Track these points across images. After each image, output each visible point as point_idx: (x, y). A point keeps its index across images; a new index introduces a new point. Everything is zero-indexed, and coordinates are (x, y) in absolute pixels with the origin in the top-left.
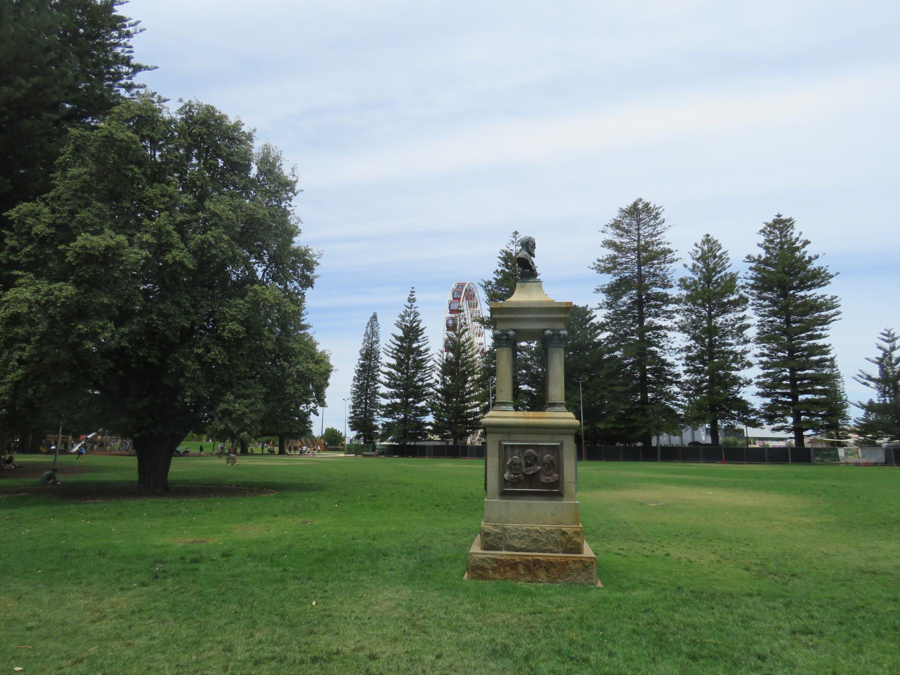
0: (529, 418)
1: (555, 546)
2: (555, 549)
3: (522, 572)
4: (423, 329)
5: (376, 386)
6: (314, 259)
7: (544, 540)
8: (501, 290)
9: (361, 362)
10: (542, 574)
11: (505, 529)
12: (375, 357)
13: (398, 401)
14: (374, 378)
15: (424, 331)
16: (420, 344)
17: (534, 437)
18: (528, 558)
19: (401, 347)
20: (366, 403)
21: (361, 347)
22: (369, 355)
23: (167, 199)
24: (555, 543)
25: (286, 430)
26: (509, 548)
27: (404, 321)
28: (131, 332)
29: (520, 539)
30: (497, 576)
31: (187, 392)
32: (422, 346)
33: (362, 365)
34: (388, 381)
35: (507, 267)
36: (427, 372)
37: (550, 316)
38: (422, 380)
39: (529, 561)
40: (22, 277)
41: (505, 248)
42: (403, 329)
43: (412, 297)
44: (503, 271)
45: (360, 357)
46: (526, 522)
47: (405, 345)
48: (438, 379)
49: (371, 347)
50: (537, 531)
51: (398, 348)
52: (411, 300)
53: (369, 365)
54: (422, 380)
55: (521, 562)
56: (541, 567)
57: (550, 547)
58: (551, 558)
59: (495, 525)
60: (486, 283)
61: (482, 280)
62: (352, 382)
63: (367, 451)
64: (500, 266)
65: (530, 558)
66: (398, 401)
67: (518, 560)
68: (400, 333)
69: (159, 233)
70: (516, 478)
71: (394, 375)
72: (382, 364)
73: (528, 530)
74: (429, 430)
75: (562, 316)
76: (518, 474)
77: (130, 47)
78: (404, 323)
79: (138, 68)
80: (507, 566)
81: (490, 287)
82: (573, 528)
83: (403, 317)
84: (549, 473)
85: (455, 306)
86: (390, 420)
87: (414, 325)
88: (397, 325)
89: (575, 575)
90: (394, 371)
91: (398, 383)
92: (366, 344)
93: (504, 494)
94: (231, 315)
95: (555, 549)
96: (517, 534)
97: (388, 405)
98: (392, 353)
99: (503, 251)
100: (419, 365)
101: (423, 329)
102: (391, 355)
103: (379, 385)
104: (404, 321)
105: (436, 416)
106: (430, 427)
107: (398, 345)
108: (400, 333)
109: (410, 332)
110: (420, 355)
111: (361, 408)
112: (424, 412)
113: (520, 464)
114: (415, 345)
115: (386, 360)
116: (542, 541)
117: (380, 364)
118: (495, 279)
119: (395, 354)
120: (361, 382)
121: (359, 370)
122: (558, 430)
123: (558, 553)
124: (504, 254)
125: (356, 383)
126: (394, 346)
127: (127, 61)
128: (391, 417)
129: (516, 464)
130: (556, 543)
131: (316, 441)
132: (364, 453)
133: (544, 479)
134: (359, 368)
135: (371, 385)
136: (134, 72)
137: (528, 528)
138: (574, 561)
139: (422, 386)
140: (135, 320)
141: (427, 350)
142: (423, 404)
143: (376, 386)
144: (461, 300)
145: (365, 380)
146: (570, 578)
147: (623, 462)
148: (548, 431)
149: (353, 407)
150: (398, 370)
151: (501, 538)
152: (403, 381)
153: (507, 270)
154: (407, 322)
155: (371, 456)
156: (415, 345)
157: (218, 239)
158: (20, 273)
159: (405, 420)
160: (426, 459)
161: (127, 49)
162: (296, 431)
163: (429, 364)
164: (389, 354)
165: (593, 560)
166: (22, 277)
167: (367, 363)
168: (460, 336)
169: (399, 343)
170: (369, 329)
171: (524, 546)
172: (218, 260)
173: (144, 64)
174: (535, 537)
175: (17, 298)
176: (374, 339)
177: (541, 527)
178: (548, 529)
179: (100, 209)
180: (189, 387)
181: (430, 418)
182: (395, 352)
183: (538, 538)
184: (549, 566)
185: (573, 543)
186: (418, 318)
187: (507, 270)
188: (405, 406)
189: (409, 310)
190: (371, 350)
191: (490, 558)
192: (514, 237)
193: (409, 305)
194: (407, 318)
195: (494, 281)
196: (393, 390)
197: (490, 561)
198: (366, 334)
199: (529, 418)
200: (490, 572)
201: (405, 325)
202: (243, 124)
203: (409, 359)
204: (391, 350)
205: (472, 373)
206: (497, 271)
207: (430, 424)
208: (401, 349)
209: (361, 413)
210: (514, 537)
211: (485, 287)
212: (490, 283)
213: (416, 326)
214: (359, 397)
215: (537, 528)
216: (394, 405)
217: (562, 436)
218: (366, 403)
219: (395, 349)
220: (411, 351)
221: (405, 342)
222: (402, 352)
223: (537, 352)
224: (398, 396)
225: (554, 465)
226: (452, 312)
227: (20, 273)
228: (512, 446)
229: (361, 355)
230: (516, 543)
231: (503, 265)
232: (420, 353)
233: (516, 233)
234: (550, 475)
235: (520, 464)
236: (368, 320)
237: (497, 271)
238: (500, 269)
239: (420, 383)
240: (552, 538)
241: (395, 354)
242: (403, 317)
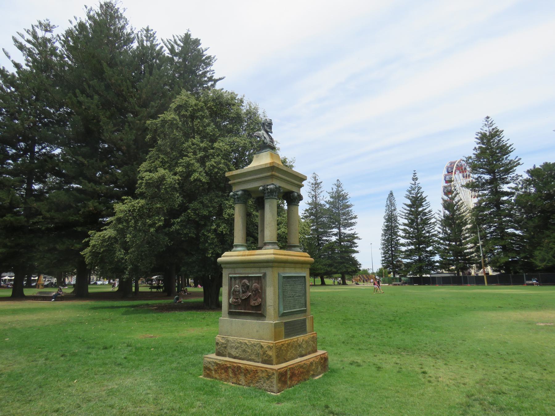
0: (245, 255)
1: (256, 357)
2: (257, 359)
3: (231, 375)
4: (425, 197)
5: (397, 239)
6: (291, 164)
7: (250, 351)
8: (480, 161)
9: (386, 224)
10: (242, 378)
11: (228, 341)
12: (395, 220)
13: (413, 247)
14: (395, 234)
15: (426, 198)
16: (424, 208)
17: (248, 270)
18: (234, 364)
19: (411, 211)
20: (392, 251)
21: (384, 214)
22: (391, 219)
23: (195, 146)
24: (256, 354)
25: (345, 270)
26: (230, 356)
27: (411, 194)
28: (181, 221)
29: (236, 349)
30: (217, 376)
31: (210, 251)
32: (425, 209)
33: (387, 226)
34: (404, 235)
35: (483, 144)
36: (432, 226)
37: (261, 175)
38: (428, 232)
39: (235, 367)
40: (127, 199)
41: (479, 131)
42: (411, 200)
43: (415, 177)
44: (480, 148)
45: (385, 221)
46: (241, 336)
47: (413, 209)
48: (440, 230)
49: (391, 213)
50: (246, 343)
51: (409, 212)
52: (415, 179)
53: (391, 226)
54: (428, 232)
55: (230, 367)
56: (241, 372)
57: (253, 357)
58: (247, 366)
59: (223, 337)
60: (467, 158)
61: (464, 157)
62: (381, 238)
63: (396, 281)
64: (478, 144)
65: (235, 365)
66: (413, 247)
67: (229, 365)
68: (409, 202)
69: (188, 165)
70: (236, 302)
71: (408, 230)
72: (400, 225)
73: (241, 343)
74: (437, 266)
75: (269, 174)
76: (237, 299)
77: (213, 71)
78: (411, 195)
79: (216, 81)
80: (222, 369)
81: (470, 161)
82: (269, 343)
83: (410, 192)
84: (255, 298)
85: (448, 178)
86: (409, 261)
87: (419, 195)
88: (406, 197)
89: (262, 382)
90: (407, 228)
91: (411, 235)
92: (388, 212)
93: (231, 314)
94: (229, 205)
95: (257, 359)
96: (234, 345)
97: (406, 251)
98: (405, 216)
99: (478, 133)
100: (425, 222)
101: (425, 197)
102: (404, 217)
103: (399, 238)
104: (411, 194)
105: (441, 256)
106: (437, 264)
107: (408, 210)
108: (409, 202)
109: (416, 200)
110: (426, 216)
111: (389, 254)
112: (432, 254)
113: (239, 291)
114: (420, 209)
115: (402, 221)
116: (248, 352)
117: (398, 225)
118: (474, 154)
119: (407, 216)
120: (387, 237)
121: (385, 229)
122: (262, 264)
123: (258, 362)
124: (480, 135)
125: (384, 238)
126: (406, 211)
127: (210, 79)
128: (409, 258)
129: (236, 291)
130: (258, 355)
131: (369, 276)
132: (393, 283)
133: (252, 303)
134: (384, 228)
135: (394, 238)
136: (215, 83)
137: (241, 341)
138: (261, 370)
139: (428, 237)
140: (183, 215)
141: (430, 211)
142: (430, 248)
143: (397, 239)
144: (453, 173)
145: (390, 235)
146: (258, 384)
147: (513, 286)
148: (256, 265)
149: (384, 253)
150: (411, 227)
151: (225, 347)
152: (415, 234)
153: (484, 146)
154: (413, 194)
155: (399, 285)
156: (420, 209)
157: (219, 163)
158: (125, 197)
159: (420, 260)
160: (437, 286)
161: (212, 72)
162: (350, 270)
163: (433, 221)
164: (402, 216)
165: (274, 372)
166: (127, 199)
167: (389, 224)
168: (453, 199)
169: (408, 208)
170: (388, 202)
171: (237, 355)
172: (219, 175)
173: (221, 77)
174: (244, 348)
175: (121, 210)
176: (393, 208)
177: (249, 341)
178: (253, 342)
179: (163, 158)
180: (211, 248)
181: (437, 258)
182: (407, 215)
183: (247, 349)
184: (247, 372)
185: (267, 355)
186: (421, 190)
187: (484, 146)
188: (418, 251)
189: (414, 186)
190: (392, 216)
191: (213, 362)
192: (486, 121)
193: (413, 182)
194: (413, 192)
195: (473, 156)
196: (408, 240)
197: (213, 364)
198: (387, 206)
199: (245, 255)
200: (213, 372)
201: (412, 196)
202: (237, 95)
203: (417, 219)
204: (404, 214)
205: (466, 224)
206: (475, 148)
207: (437, 262)
208: (411, 213)
209: (389, 257)
210: (232, 347)
211: (467, 161)
212: (470, 158)
213: (420, 196)
214: (387, 247)
215: (246, 341)
216: (411, 250)
217: (265, 269)
218: (392, 251)
219: (407, 213)
220: (417, 213)
221: (414, 208)
222: (412, 215)
223: (516, 203)
224: (412, 244)
225: (259, 292)
226: (447, 182)
227: (125, 197)
228: (235, 278)
229: (386, 219)
230: (234, 353)
231: (480, 143)
232: (425, 214)
233: (488, 118)
234: (256, 300)
235: (239, 291)
236: (387, 196)
237: (475, 148)
238: (477, 146)
239: (427, 235)
240: (255, 350)
241: (407, 216)
242: (410, 192)
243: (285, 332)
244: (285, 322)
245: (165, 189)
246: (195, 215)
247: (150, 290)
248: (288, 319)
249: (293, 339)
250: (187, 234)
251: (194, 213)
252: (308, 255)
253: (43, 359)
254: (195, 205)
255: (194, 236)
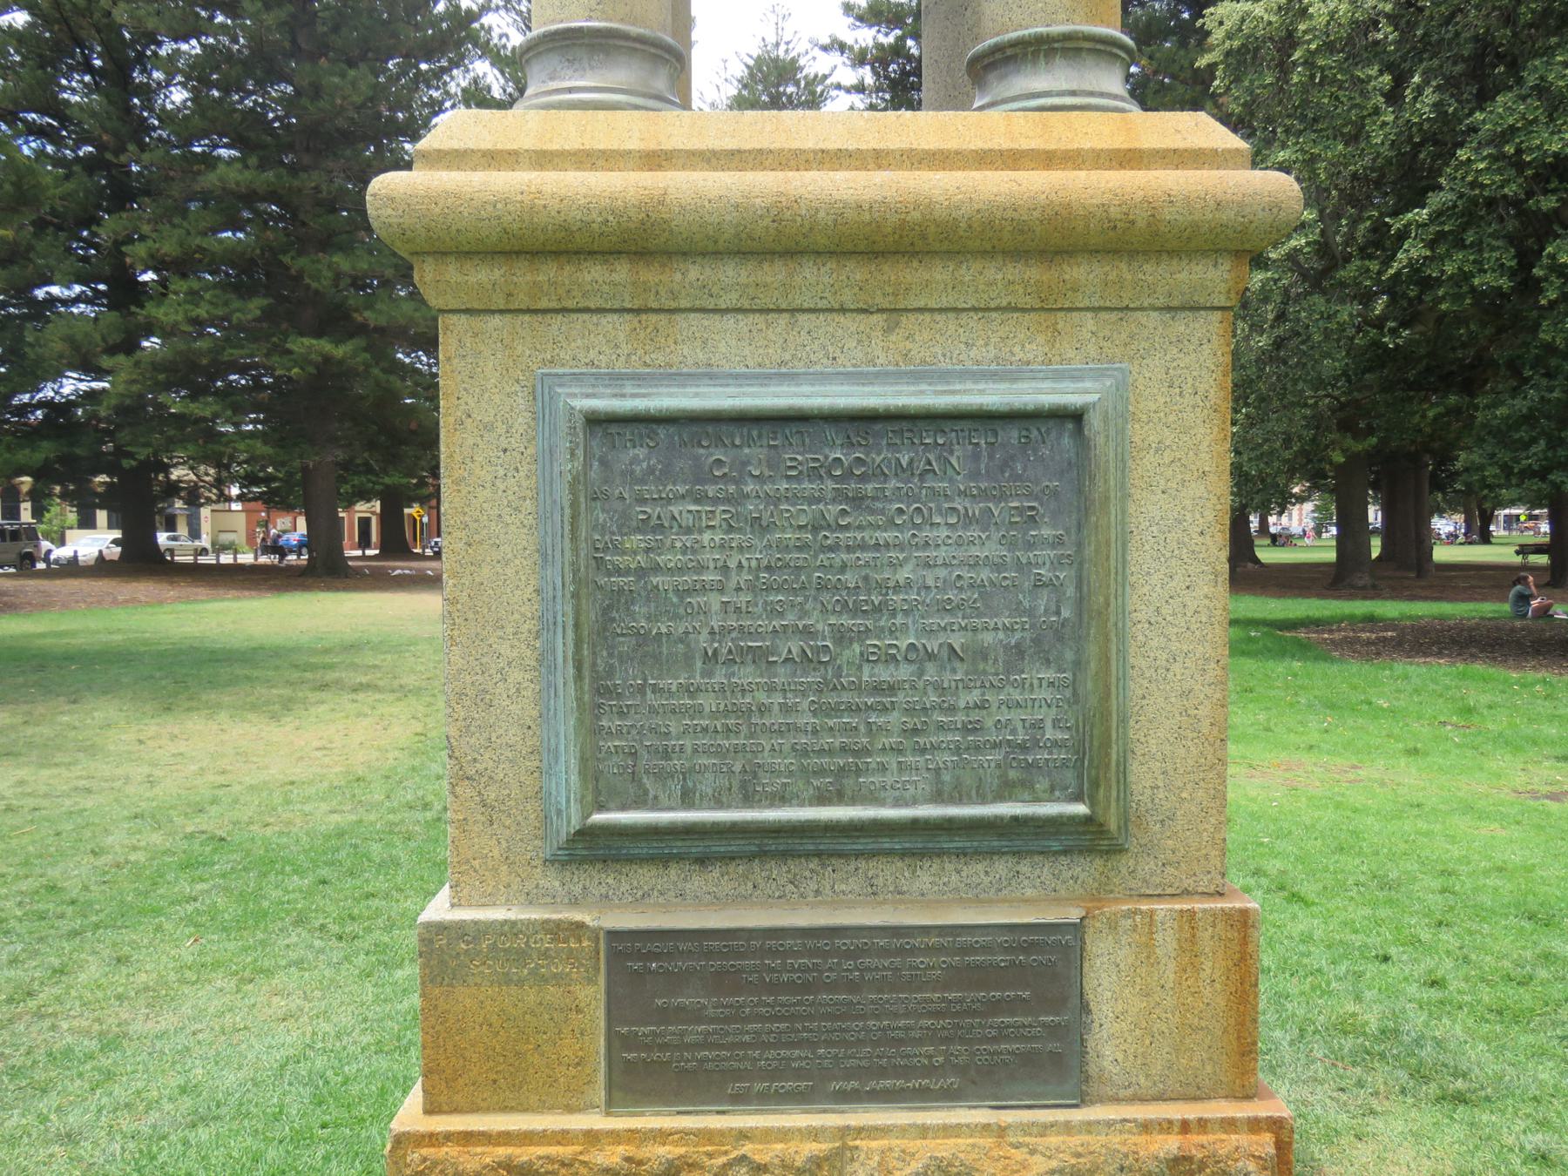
28: (1436, 217)
243: (615, 1040)
244: (613, 935)
245: (1308, 63)
246: (1499, 171)
247: (1518, 559)
248: (719, 902)
249: (743, 1135)
250: (1464, 277)
251: (1494, 158)
252: (1234, 141)
253: (1400, 746)
254: (1505, 109)
255: (1505, 283)
